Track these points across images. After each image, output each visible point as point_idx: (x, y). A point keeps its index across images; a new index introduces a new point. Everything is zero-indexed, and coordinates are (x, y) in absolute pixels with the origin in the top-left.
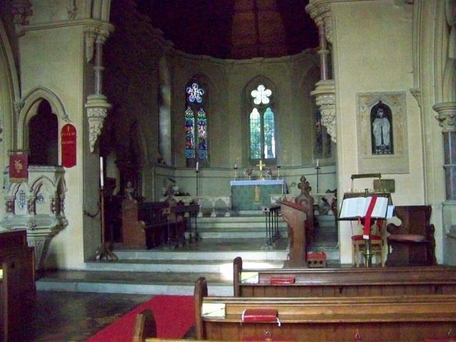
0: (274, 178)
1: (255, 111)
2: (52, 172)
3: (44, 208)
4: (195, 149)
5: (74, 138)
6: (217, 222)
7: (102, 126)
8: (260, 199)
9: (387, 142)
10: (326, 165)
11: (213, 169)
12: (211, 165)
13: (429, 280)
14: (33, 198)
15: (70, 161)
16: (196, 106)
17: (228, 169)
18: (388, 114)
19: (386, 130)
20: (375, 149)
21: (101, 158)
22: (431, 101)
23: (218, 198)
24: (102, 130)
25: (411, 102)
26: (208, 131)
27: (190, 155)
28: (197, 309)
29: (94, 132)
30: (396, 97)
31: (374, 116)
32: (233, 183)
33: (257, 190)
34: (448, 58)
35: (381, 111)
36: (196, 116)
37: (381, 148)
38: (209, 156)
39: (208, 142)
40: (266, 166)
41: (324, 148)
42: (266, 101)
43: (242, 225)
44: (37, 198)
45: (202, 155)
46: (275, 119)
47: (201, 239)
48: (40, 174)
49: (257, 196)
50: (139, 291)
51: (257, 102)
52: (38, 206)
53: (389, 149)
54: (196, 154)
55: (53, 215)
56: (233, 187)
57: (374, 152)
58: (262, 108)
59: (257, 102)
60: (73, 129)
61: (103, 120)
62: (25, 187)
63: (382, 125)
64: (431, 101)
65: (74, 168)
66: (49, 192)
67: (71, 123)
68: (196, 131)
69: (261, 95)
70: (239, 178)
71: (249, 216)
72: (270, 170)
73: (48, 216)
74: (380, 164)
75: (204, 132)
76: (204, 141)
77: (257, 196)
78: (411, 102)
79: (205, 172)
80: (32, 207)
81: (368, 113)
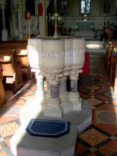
0: (90, 20)
2: (37, 17)
3: (35, 28)
4: (63, 10)
5: (42, 7)
6: (75, 34)
7: (49, 3)
8: (86, 27)
10: (108, 16)
12: (68, 15)
13: (16, 25)
14: (32, 25)
15: (40, 14)
17: (74, 17)
21: (50, 14)
23: (74, 26)
24: (49, 5)
26: (67, 3)
27: (62, 11)
29: (47, 5)
32: (77, 21)
38: (68, 12)
39: (67, 7)
40: (88, 16)
41: (107, 10)
43: (87, 35)
44: (33, 25)
45: (66, 11)
47: (73, 40)
48: (34, 18)
49: (85, 26)
52: (33, 27)
54: (64, 11)
55: (37, 30)
56: (77, 23)
60: (41, 4)
61: (50, 2)
62: (29, 22)
65: (42, 16)
66: (36, 23)
67: (41, 3)
70: (79, 20)
71: (85, 32)
72: (89, 17)
73: (36, 30)
75: (66, 4)
76: (66, 6)
77: (85, 26)
79: (67, 18)
80: (32, 27)
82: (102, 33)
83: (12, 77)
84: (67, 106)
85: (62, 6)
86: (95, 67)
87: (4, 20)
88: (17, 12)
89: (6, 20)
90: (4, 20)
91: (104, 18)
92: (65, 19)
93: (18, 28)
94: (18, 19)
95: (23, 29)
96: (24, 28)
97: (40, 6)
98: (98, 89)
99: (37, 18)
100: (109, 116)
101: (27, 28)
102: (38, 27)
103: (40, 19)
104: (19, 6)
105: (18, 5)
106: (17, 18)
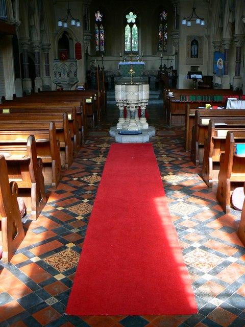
1: (128, 27)
3: (72, 75)
9: (196, 53)
11: (113, 56)
16: (99, 23)
18: (197, 44)
19: (196, 49)
20: (192, 56)
22: (212, 40)
25: (205, 39)
28: (7, 107)
30: (200, 38)
31: (192, 44)
33: (235, 138)
34: (219, 27)
35: (195, 42)
36: (99, 29)
37: (194, 55)
42: (134, 21)
46: (138, 31)
50: (133, 141)
51: (129, 21)
53: (197, 56)
57: (191, 57)
58: (131, 25)
59: (129, 21)
60: (80, 45)
63: (195, 48)
64: (212, 40)
68: (99, 37)
69: (131, 18)
70: (123, 61)
74: (194, 62)
78: (205, 39)
79: (105, 58)
81: (190, 42)
82: (158, 81)
83: (25, 144)
84: (210, 114)
85: (97, 42)
86: (93, 160)
87: (26, 61)
88: (48, 54)
89: (29, 65)
90: (26, 61)
91: (159, 58)
92: (102, 60)
93: (49, 75)
94: (48, 63)
95: (55, 76)
96: (58, 75)
97: (78, 47)
98: (173, 161)
99: (74, 63)
100: (176, 294)
101: (62, 75)
102: (75, 75)
103: (77, 63)
104: (50, 47)
105: (50, 45)
106: (48, 62)
